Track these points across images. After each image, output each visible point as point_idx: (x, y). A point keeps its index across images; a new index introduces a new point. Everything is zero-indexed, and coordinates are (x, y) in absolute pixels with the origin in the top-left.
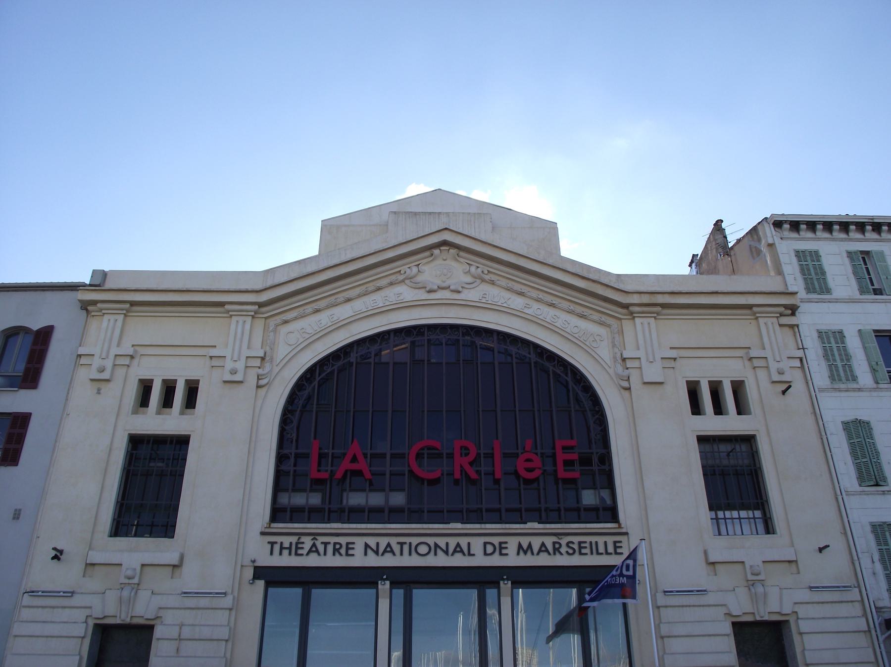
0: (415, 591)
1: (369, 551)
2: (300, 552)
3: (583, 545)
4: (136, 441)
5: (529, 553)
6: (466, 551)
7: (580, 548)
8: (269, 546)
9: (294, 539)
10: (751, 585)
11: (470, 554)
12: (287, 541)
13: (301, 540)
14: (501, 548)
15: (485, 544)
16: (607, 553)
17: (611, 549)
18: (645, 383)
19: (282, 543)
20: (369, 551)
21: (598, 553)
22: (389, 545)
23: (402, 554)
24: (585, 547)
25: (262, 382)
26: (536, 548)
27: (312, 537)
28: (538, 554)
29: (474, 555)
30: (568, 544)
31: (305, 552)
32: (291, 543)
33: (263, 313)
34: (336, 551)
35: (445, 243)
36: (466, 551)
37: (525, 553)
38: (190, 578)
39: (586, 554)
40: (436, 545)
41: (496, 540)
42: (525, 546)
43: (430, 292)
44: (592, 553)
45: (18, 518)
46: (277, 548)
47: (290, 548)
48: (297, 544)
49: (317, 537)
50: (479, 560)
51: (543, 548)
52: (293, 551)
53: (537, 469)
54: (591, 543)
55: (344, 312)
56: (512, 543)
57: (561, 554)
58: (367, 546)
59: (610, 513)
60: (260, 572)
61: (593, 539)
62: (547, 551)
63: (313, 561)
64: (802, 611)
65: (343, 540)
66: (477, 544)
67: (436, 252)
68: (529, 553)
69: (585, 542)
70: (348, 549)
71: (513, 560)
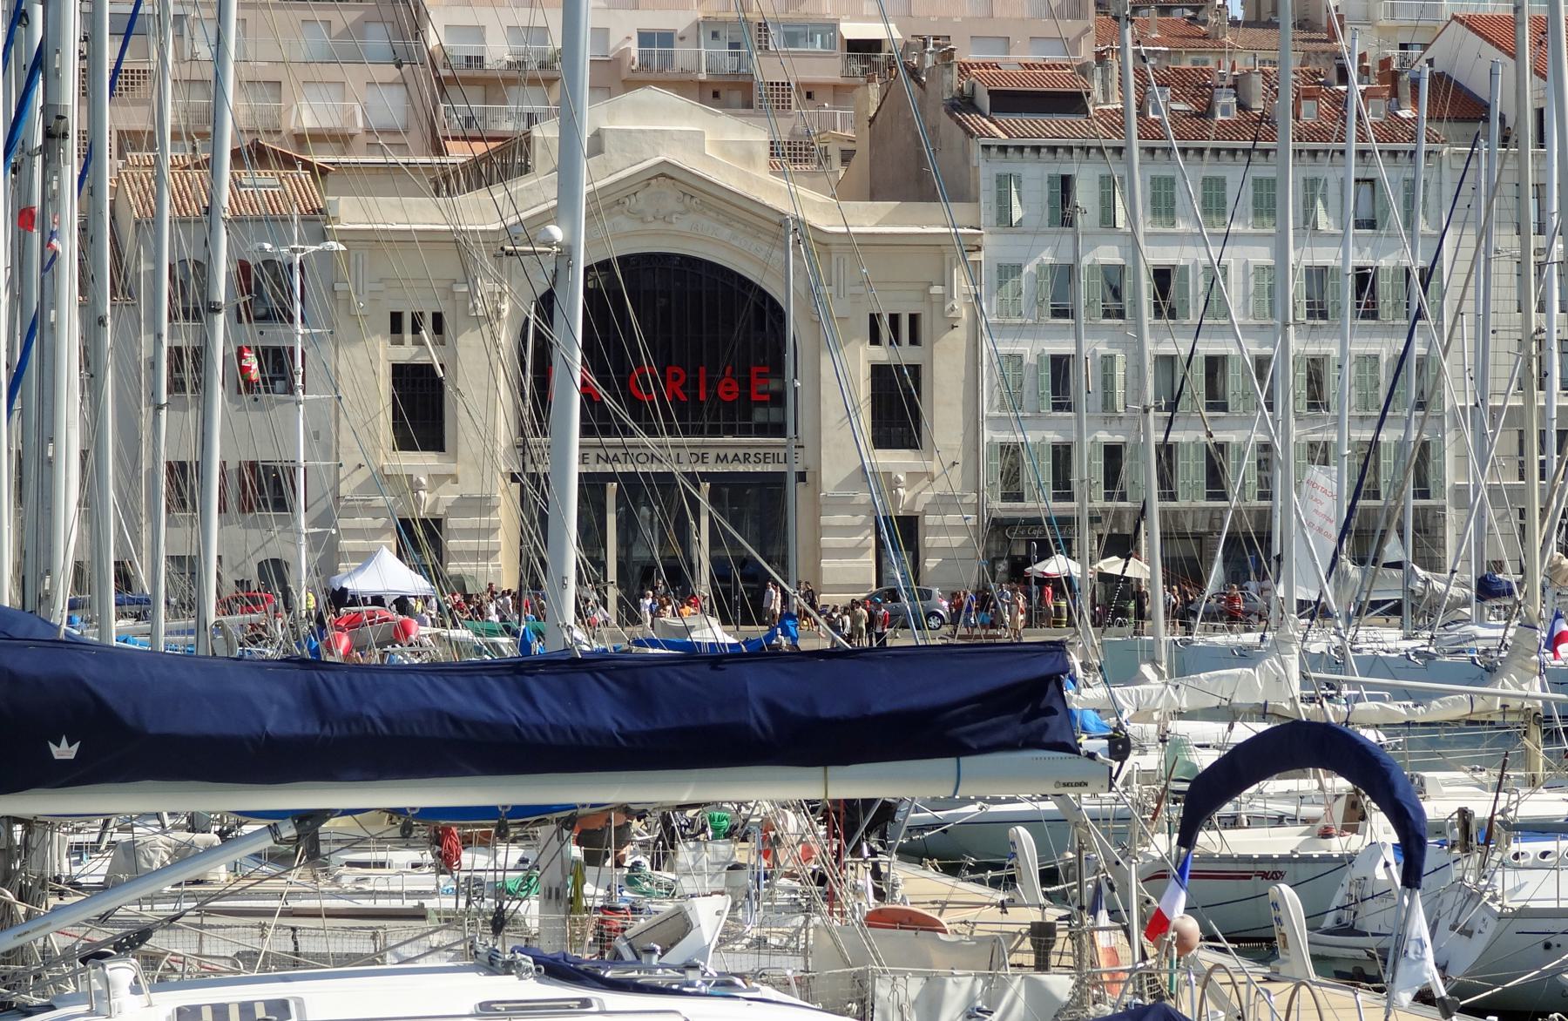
26: (730, 458)
35: (663, 175)
61: (776, 451)
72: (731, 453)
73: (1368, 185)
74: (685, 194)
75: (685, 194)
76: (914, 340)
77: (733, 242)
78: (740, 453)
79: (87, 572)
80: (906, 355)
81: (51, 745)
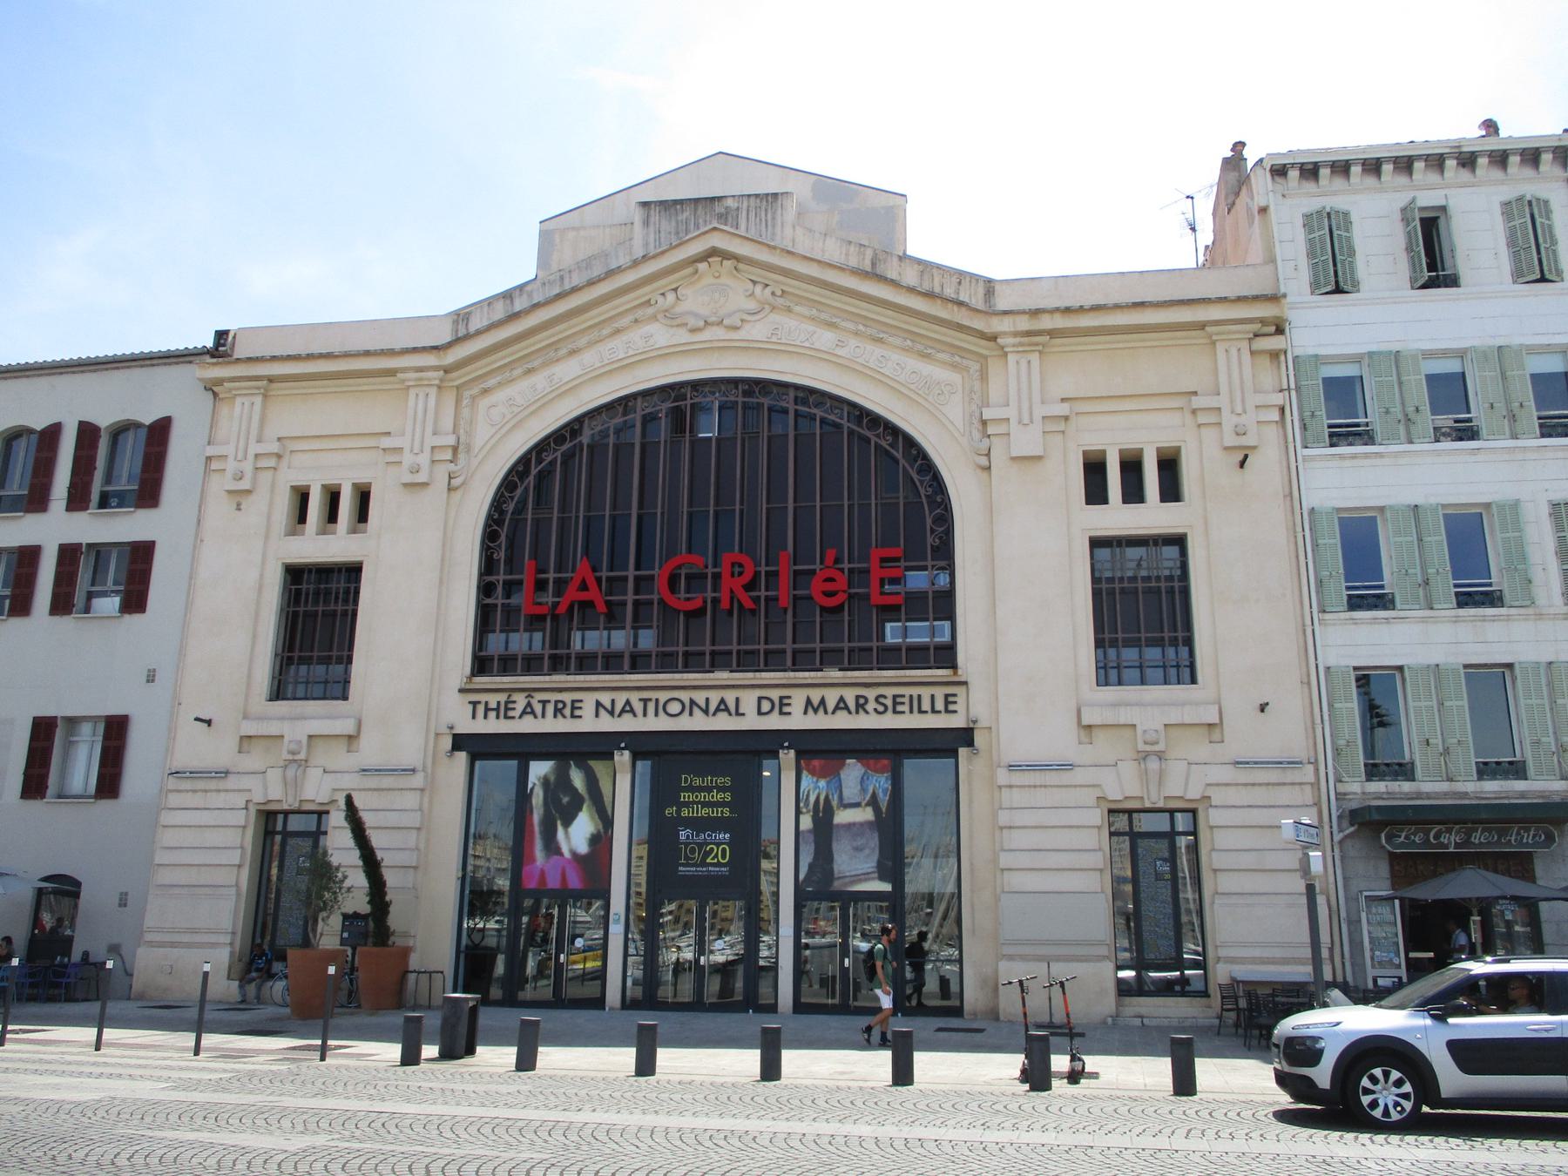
0: (907, 762)
1: (602, 712)
2: (511, 713)
3: (899, 700)
4: (294, 573)
5: (821, 711)
6: (733, 710)
7: (895, 704)
8: (471, 707)
9: (502, 697)
10: (1143, 757)
11: (738, 714)
12: (493, 700)
13: (512, 699)
14: (782, 705)
15: (760, 699)
16: (934, 711)
17: (940, 705)
18: (1014, 459)
19: (486, 703)
20: (602, 711)
21: (920, 711)
22: (628, 702)
23: (645, 714)
24: (903, 703)
25: (455, 482)
26: (831, 705)
27: (526, 694)
28: (833, 713)
29: (743, 714)
30: (877, 700)
31: (516, 713)
32: (499, 703)
33: (452, 380)
34: (558, 712)
36: (733, 710)
37: (816, 711)
38: (371, 751)
39: (903, 712)
40: (692, 702)
41: (775, 694)
42: (816, 701)
43: (693, 331)
44: (911, 711)
45: (153, 681)
46: (481, 709)
47: (497, 710)
48: (507, 703)
49: (533, 694)
50: (751, 721)
51: (841, 705)
52: (505, 711)
53: (840, 593)
54: (911, 696)
55: (567, 370)
56: (798, 699)
57: (867, 712)
58: (598, 704)
59: (946, 655)
60: (460, 742)
61: (915, 691)
62: (847, 708)
63: (528, 726)
64: (1217, 797)
65: (567, 697)
66: (749, 700)
67: (702, 266)
68: (821, 711)
69: (903, 696)
70: (573, 708)
71: (798, 720)
72: (832, 697)
73: (1190, 815)
74: (754, 283)
75: (754, 283)
77: (839, 352)
78: (850, 695)
79: (222, 785)
81: (559, 823)
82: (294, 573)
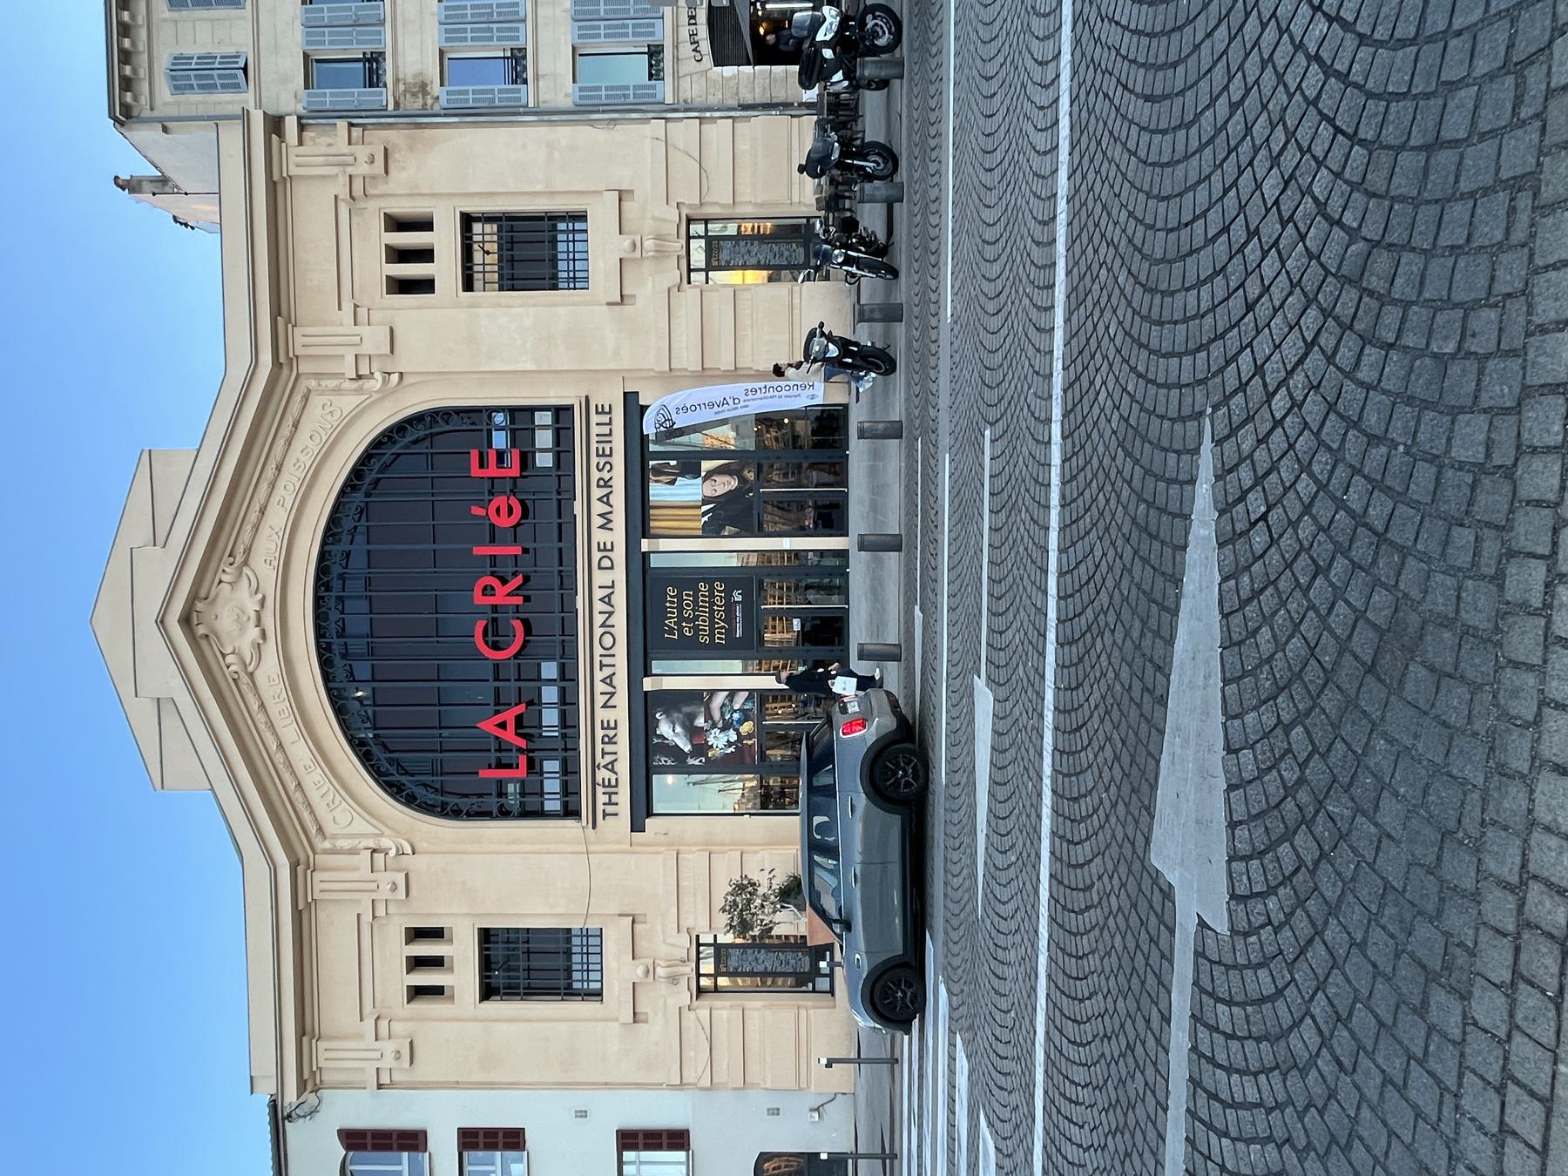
4: (488, 992)
12: (602, 799)
26: (605, 509)
35: (186, 621)
51: (605, 500)
61: (594, 439)
66: (600, 578)
76: (426, 225)
80: (445, 240)
82: (488, 992)
